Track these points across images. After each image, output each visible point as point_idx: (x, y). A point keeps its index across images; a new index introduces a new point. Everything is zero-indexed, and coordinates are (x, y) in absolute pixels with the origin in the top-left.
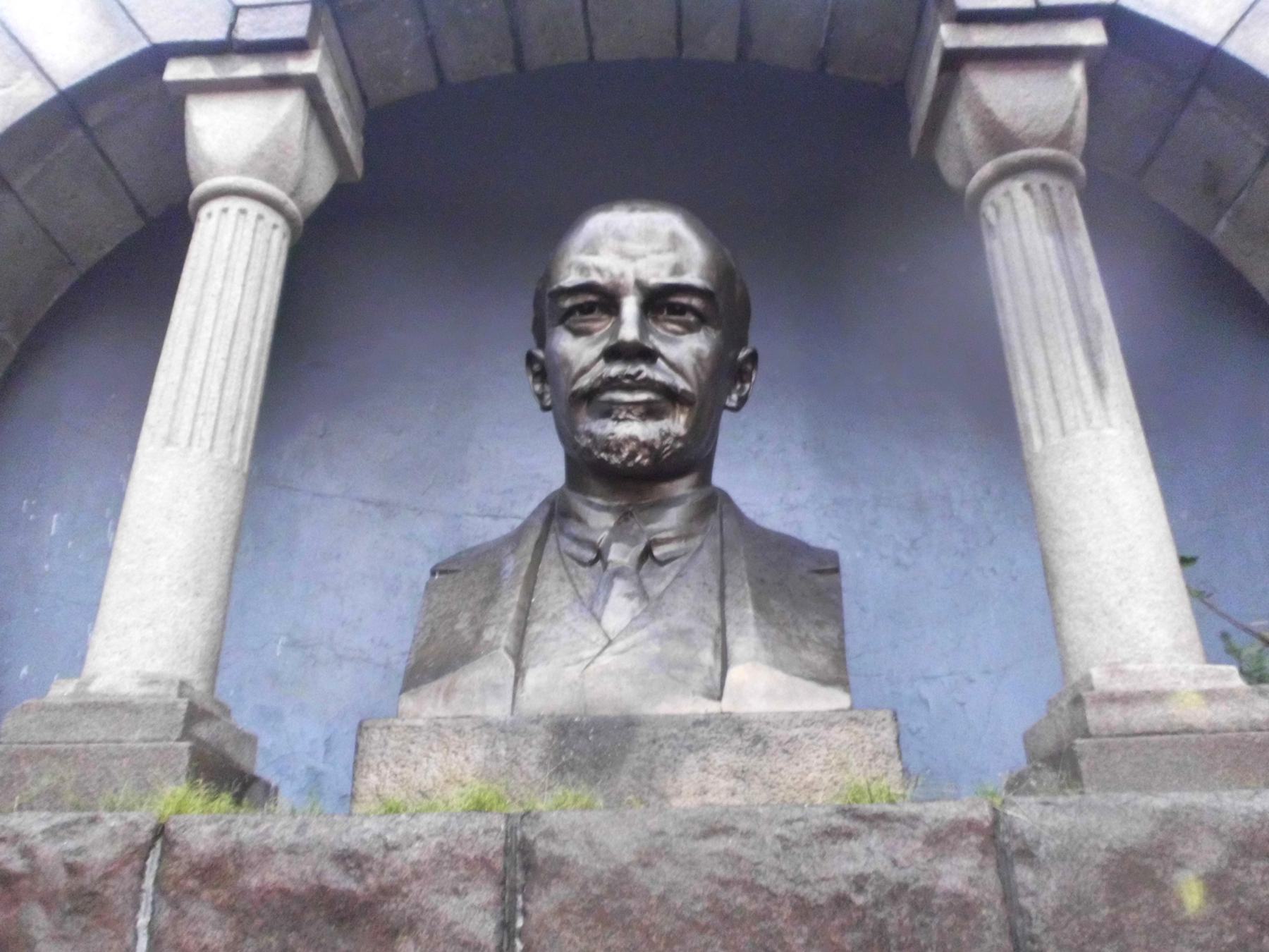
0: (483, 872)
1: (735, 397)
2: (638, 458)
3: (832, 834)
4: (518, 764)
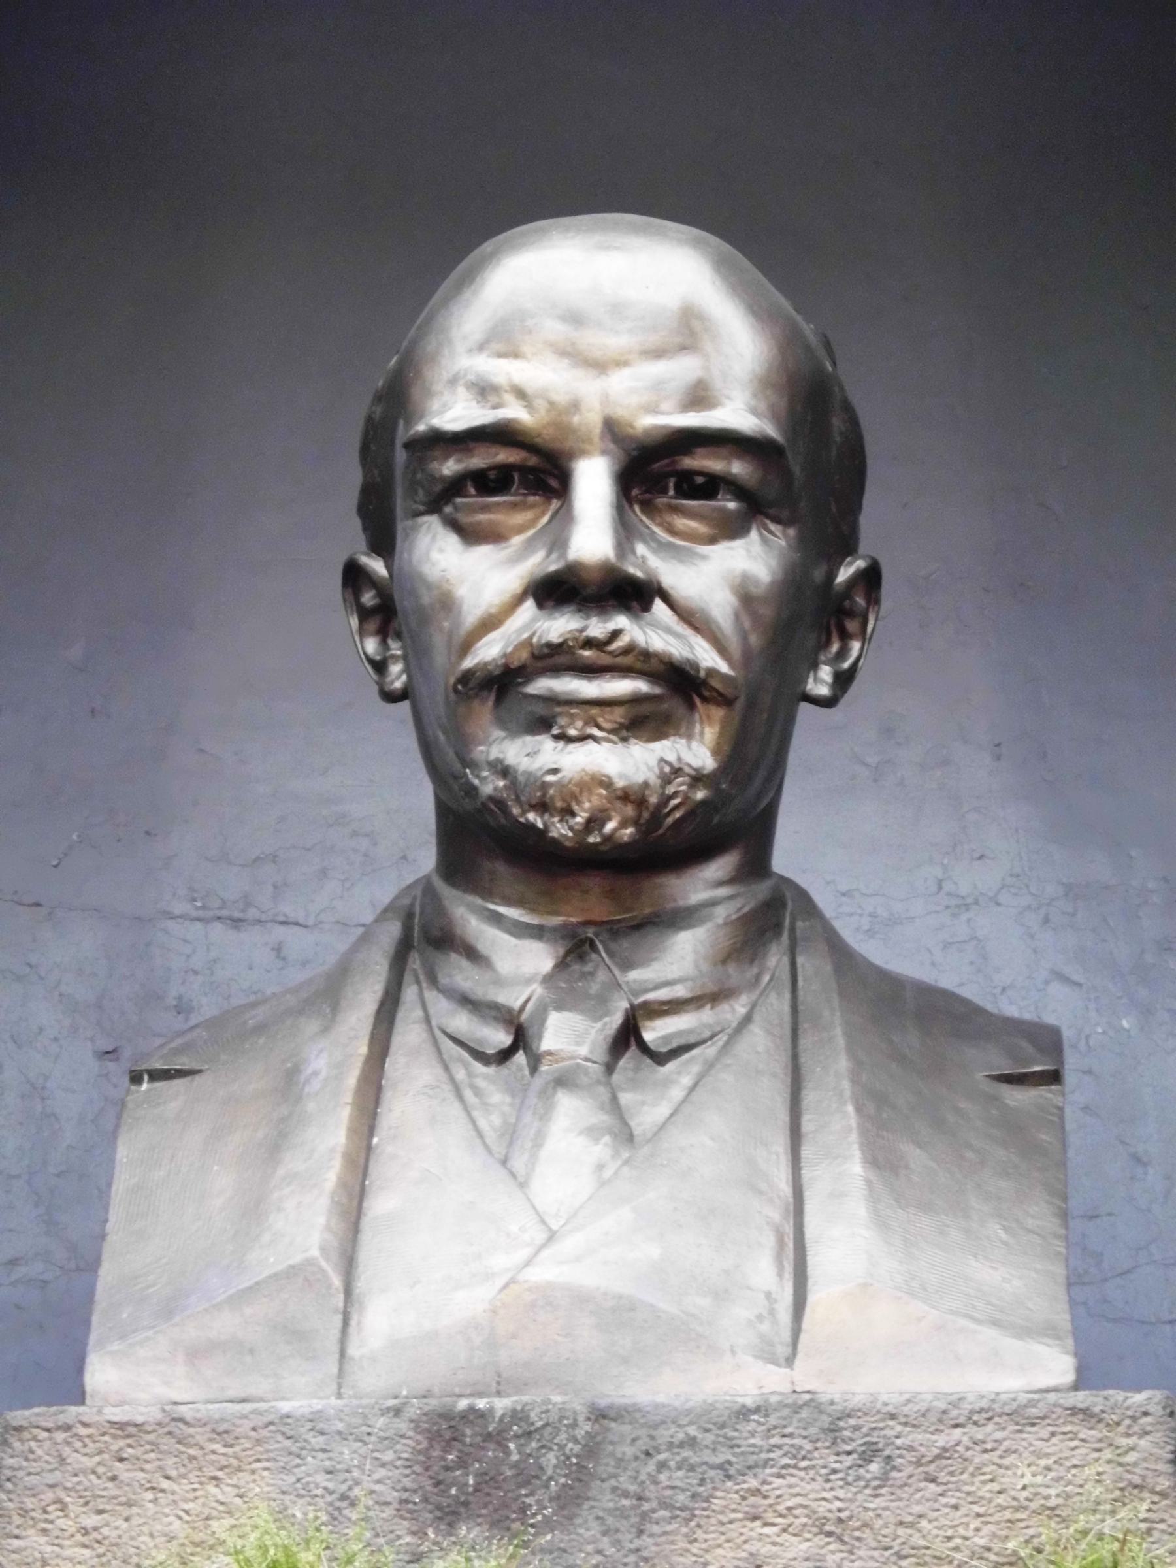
1: (826, 673)
2: (610, 826)
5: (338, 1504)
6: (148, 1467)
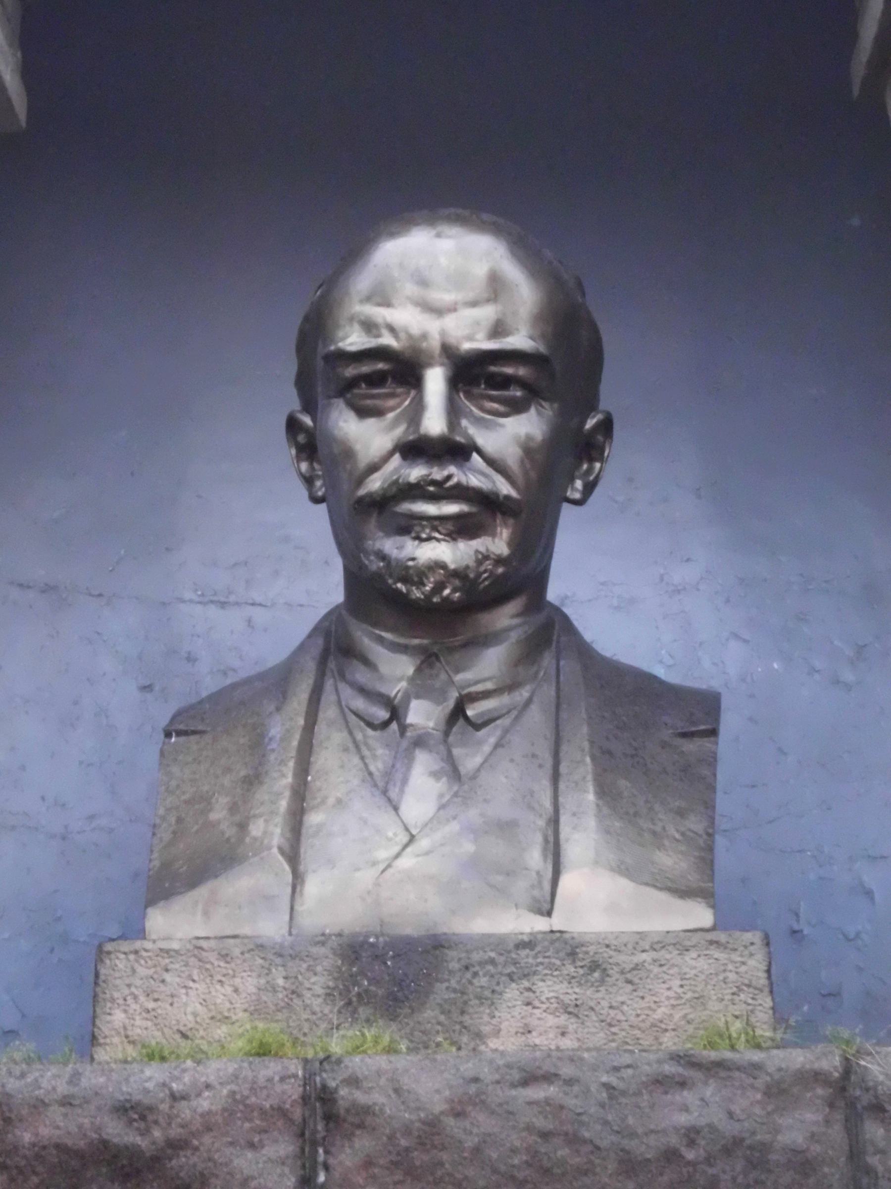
0: (280, 1123)
1: (579, 484)
2: (447, 592)
3: (661, 1082)
4: (299, 996)
5: (290, 996)
6: (182, 975)
